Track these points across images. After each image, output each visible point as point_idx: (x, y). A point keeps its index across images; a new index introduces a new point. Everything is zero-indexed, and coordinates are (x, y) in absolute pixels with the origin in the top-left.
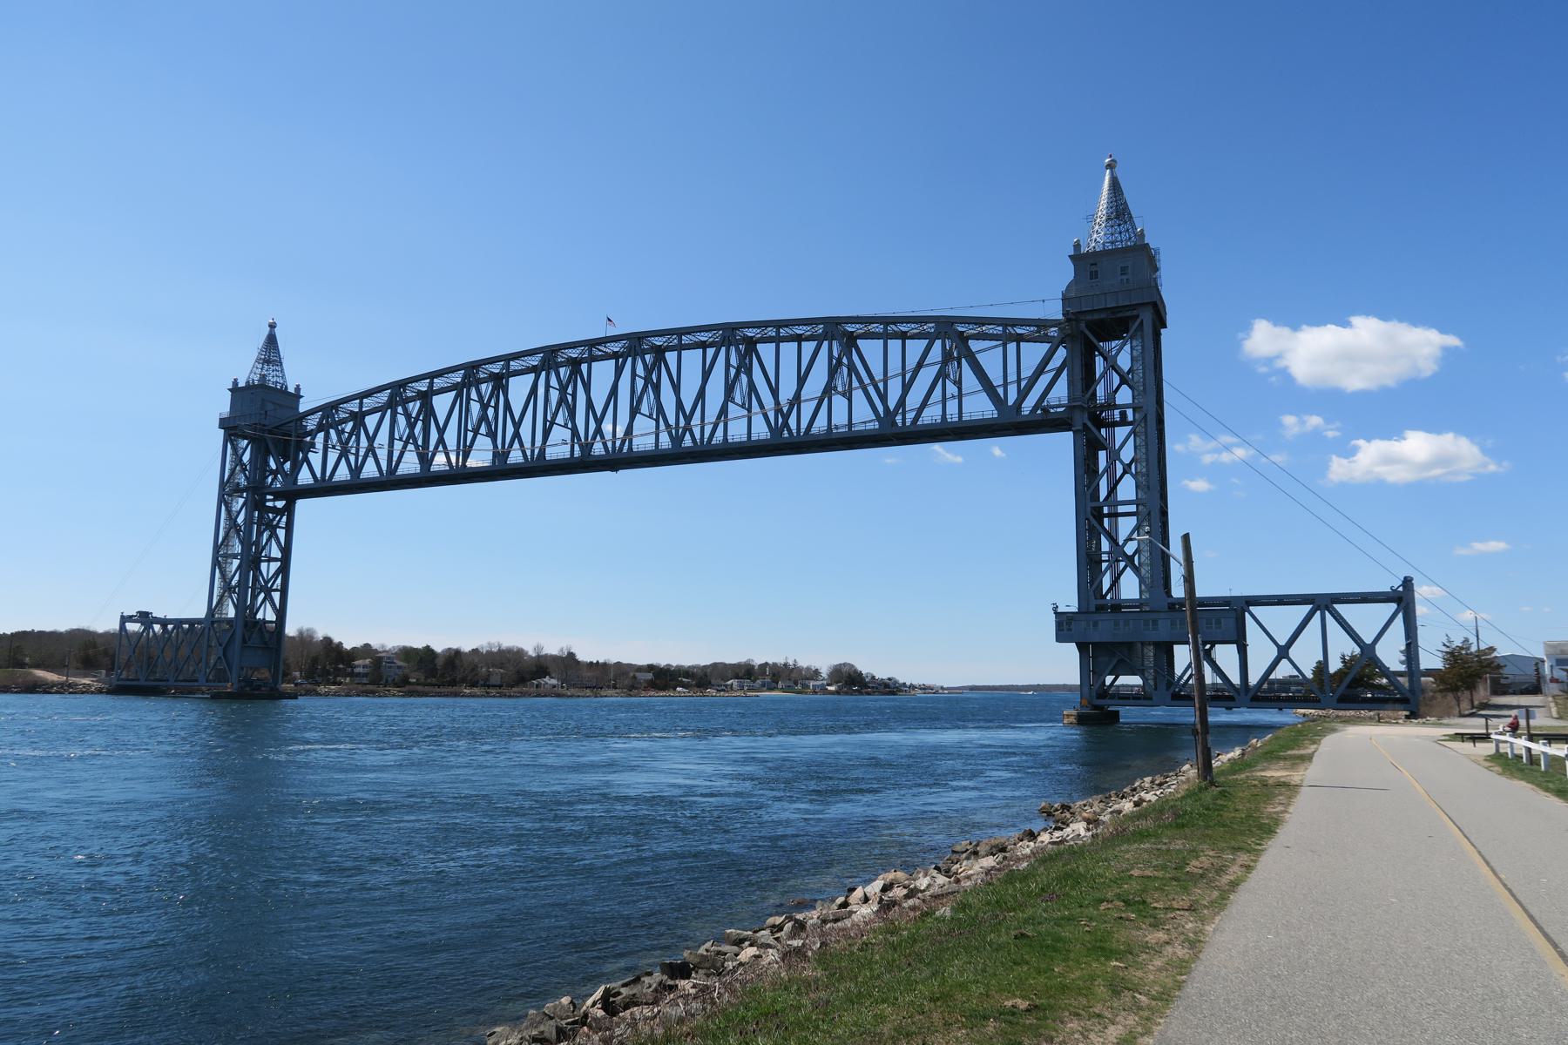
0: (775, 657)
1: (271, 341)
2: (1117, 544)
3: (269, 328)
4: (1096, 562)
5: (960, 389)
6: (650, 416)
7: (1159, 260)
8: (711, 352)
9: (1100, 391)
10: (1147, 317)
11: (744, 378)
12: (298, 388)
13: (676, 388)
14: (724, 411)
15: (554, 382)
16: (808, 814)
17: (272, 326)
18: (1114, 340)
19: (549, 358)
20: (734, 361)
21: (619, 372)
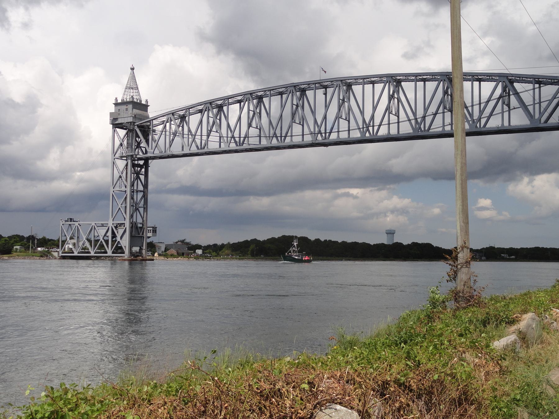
5: (509, 107)
6: (257, 128)
8: (285, 96)
11: (346, 104)
12: (147, 101)
13: (268, 114)
14: (290, 127)
15: (211, 115)
19: (209, 105)
21: (241, 109)
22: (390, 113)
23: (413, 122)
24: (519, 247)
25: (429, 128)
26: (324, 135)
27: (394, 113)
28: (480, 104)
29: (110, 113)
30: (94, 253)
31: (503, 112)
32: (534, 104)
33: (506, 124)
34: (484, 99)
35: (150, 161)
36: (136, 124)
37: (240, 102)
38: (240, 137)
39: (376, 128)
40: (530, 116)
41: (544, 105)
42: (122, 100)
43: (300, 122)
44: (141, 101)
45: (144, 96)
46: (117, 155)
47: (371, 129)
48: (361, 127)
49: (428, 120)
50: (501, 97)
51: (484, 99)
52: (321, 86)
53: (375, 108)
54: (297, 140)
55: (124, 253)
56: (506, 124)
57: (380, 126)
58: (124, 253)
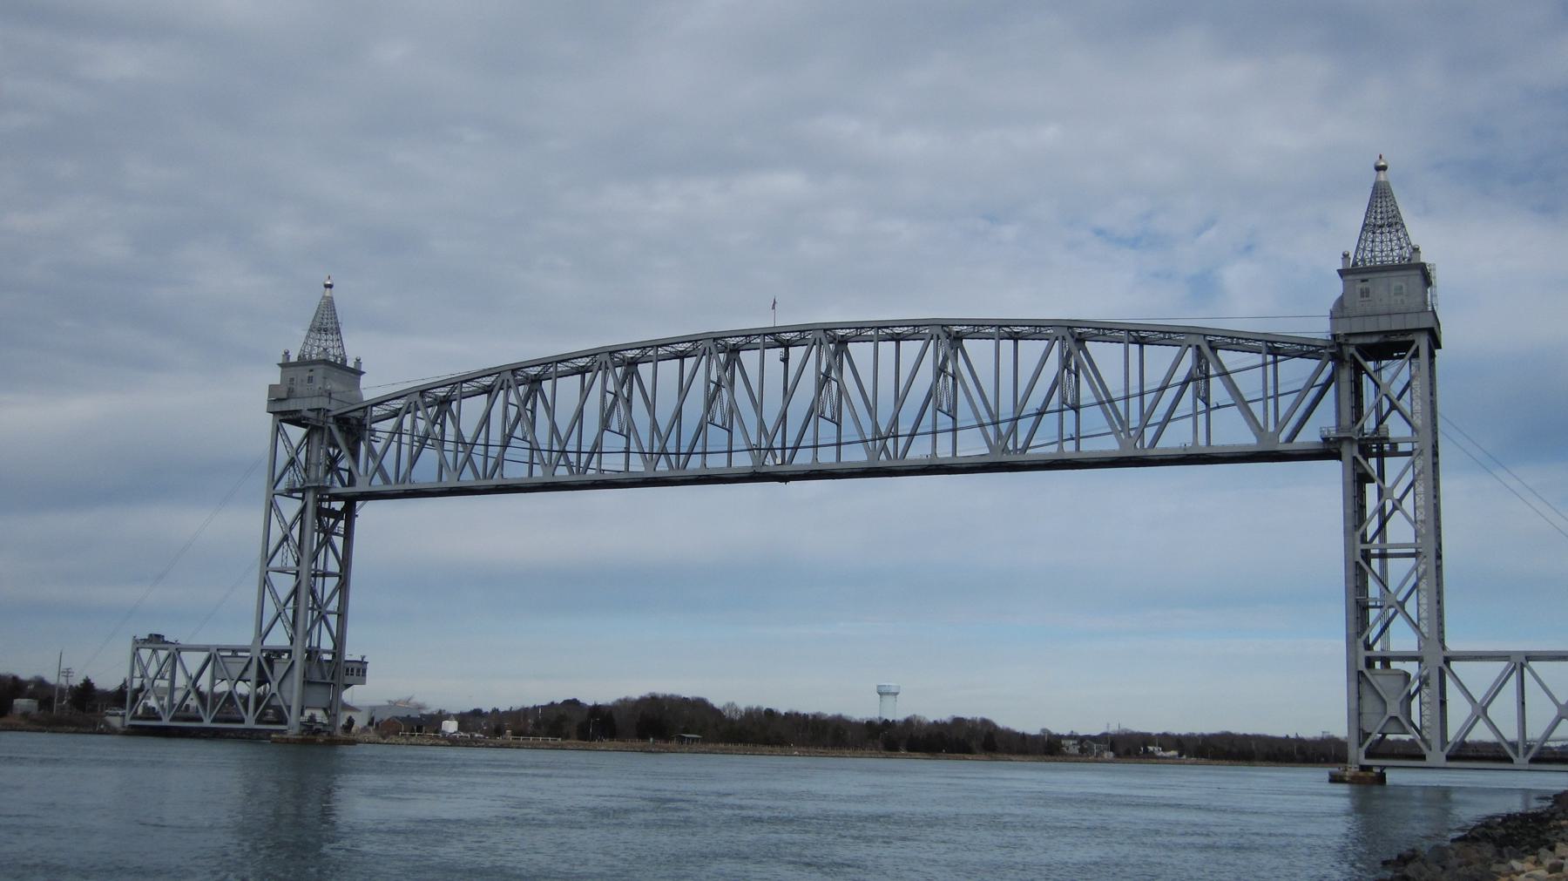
0: (636, 689)
1: (1381, 193)
5: (1207, 404)
6: (620, 433)
7: (1435, 278)
8: (689, 363)
9: (1370, 424)
10: (1423, 342)
13: (651, 406)
14: (701, 428)
18: (1383, 360)
25: (1027, 446)
28: (1142, 394)
29: (270, 386)
30: (171, 720)
40: (1259, 430)
42: (299, 357)
44: (344, 360)
57: (912, 435)
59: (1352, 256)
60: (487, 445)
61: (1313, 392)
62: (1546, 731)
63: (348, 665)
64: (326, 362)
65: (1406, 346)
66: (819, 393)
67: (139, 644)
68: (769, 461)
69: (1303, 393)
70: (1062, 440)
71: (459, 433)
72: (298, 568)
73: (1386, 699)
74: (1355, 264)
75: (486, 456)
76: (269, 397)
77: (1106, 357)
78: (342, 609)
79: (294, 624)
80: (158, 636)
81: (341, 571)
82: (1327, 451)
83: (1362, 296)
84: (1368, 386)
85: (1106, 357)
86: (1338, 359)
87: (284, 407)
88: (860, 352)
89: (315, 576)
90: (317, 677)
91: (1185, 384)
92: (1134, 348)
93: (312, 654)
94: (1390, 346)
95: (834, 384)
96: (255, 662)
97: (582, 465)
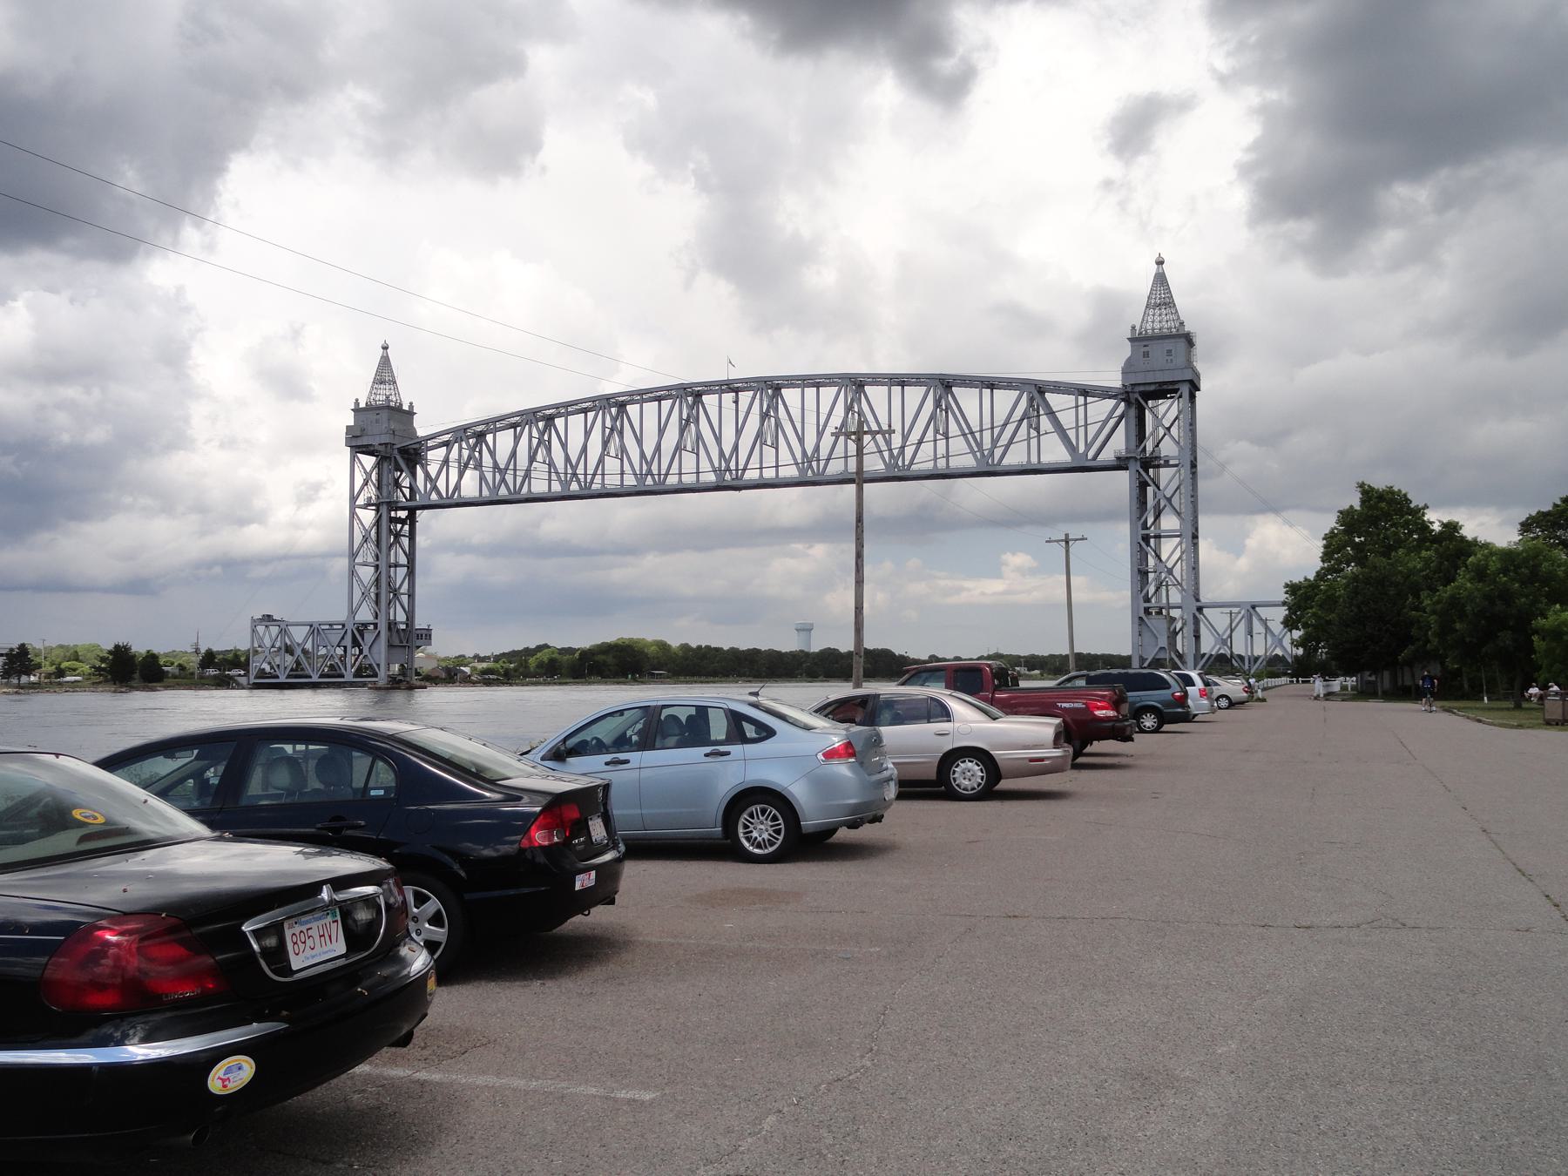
1: (385, 363)
2: (1161, 560)
3: (1156, 266)
4: (1144, 573)
5: (1038, 432)
6: (616, 457)
8: (591, 415)
9: (1149, 445)
13: (564, 446)
14: (601, 461)
16: (463, 772)
17: (1160, 263)
20: (608, 424)
22: (764, 443)
23: (886, 454)
24: (1046, 654)
25: (911, 463)
26: (734, 472)
27: (769, 443)
28: (992, 428)
29: (347, 427)
30: (319, 677)
31: (1029, 439)
32: (1077, 427)
33: (1034, 460)
34: (999, 419)
35: (418, 512)
36: (395, 447)
37: (514, 426)
38: (586, 474)
39: (822, 463)
40: (1072, 448)
41: (1092, 430)
42: (367, 403)
43: (617, 455)
44: (401, 405)
45: (407, 395)
46: (361, 501)
47: (814, 464)
48: (800, 461)
49: (909, 451)
50: (1025, 416)
51: (999, 421)
52: (730, 388)
53: (739, 432)
54: (612, 481)
55: (376, 675)
56: (1034, 460)
57: (828, 460)
58: (376, 675)
59: (1138, 328)
60: (515, 470)
61: (1112, 422)
62: (662, 683)
63: (419, 632)
64: (389, 407)
65: (1176, 391)
66: (762, 424)
67: (255, 623)
68: (728, 477)
69: (1105, 422)
70: (935, 459)
71: (495, 463)
72: (377, 563)
73: (1158, 636)
74: (1140, 334)
75: (515, 476)
76: (347, 434)
77: (967, 399)
78: (411, 590)
79: (377, 602)
80: (269, 616)
81: (408, 563)
82: (1120, 464)
83: (1144, 357)
84: (1148, 416)
85: (967, 399)
86: (1127, 401)
87: (359, 443)
88: (791, 395)
89: (390, 567)
90: (397, 642)
91: (1021, 421)
92: (987, 392)
93: (392, 625)
94: (1163, 391)
95: (773, 420)
96: (349, 633)
97: (588, 481)
